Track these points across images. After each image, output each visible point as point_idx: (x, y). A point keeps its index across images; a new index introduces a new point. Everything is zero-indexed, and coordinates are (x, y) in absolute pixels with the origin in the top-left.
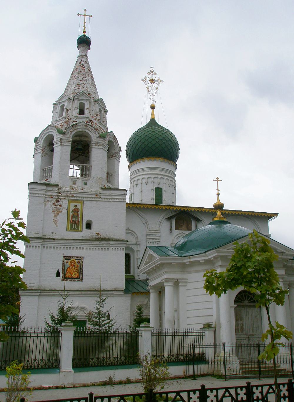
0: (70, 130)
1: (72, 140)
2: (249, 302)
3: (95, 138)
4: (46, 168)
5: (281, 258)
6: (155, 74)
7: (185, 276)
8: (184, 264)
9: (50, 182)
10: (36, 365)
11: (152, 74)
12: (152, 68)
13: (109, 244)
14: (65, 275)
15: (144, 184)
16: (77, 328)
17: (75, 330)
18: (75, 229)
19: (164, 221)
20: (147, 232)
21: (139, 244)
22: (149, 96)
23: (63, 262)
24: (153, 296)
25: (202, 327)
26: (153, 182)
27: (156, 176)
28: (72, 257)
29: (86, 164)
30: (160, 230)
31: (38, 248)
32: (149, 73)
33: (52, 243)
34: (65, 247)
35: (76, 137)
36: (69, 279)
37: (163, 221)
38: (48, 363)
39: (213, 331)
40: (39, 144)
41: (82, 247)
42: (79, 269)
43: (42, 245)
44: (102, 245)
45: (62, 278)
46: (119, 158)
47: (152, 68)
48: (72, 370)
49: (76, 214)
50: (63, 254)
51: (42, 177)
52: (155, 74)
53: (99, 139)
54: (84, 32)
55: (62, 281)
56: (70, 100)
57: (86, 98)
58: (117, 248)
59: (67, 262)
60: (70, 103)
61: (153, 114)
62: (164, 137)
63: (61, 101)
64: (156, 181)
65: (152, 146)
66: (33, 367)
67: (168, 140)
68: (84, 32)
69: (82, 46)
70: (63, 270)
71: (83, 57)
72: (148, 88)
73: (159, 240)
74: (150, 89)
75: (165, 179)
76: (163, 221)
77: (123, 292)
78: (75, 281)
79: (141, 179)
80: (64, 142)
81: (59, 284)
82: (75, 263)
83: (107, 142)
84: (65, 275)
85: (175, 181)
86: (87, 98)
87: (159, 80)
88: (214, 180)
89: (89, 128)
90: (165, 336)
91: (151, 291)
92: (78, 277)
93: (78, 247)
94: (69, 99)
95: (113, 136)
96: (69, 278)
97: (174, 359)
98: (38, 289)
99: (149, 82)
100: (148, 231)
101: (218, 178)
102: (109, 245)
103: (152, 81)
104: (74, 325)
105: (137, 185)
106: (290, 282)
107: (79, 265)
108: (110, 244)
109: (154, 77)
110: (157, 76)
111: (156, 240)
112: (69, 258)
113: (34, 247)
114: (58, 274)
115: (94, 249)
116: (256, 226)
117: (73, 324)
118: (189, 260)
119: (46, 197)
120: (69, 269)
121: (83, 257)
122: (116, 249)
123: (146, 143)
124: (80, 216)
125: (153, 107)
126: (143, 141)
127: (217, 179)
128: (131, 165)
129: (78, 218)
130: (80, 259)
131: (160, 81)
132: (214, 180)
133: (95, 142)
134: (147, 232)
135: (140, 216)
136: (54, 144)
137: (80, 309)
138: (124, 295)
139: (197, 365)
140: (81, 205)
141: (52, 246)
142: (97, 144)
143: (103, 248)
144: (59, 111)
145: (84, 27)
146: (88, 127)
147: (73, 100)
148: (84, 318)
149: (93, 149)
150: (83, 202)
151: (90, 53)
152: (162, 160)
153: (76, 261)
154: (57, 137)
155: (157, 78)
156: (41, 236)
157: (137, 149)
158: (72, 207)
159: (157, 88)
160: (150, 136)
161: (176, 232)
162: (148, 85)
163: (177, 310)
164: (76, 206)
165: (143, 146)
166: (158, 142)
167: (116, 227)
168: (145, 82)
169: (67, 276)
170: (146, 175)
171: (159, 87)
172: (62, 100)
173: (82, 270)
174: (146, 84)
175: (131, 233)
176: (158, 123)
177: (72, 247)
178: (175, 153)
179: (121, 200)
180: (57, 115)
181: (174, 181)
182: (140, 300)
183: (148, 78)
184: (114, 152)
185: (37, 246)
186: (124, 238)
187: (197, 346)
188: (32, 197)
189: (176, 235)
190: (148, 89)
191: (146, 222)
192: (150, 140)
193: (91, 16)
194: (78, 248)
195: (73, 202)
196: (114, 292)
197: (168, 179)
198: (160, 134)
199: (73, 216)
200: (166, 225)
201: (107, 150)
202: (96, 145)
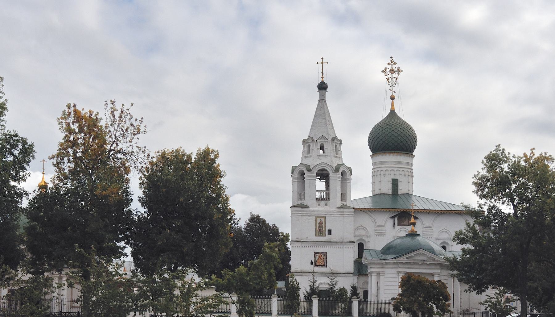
4: (301, 192)
6: (395, 64)
7: (384, 270)
8: (383, 263)
12: (392, 58)
15: (382, 176)
18: (320, 235)
22: (389, 87)
27: (382, 169)
28: (320, 252)
32: (389, 64)
36: (318, 266)
41: (325, 246)
42: (325, 260)
48: (318, 316)
49: (321, 225)
51: (299, 199)
52: (395, 64)
54: (322, 78)
58: (348, 247)
61: (393, 105)
64: (392, 173)
68: (322, 78)
71: (322, 100)
72: (388, 79)
73: (385, 234)
74: (390, 80)
75: (401, 171)
78: (322, 267)
79: (380, 171)
81: (311, 268)
84: (316, 264)
87: (398, 70)
91: (369, 275)
96: (318, 265)
99: (389, 73)
103: (392, 71)
107: (324, 257)
114: (312, 263)
115: (333, 247)
118: (384, 262)
121: (326, 253)
123: (383, 140)
125: (393, 98)
126: (381, 138)
130: (325, 254)
131: (400, 71)
135: (371, 216)
141: (307, 246)
145: (322, 73)
151: (327, 94)
155: (396, 68)
157: (378, 133)
158: (318, 221)
159: (397, 79)
160: (387, 133)
161: (397, 227)
162: (388, 76)
164: (321, 220)
167: (348, 233)
171: (398, 77)
173: (326, 261)
181: (409, 170)
186: (352, 240)
189: (398, 230)
190: (388, 80)
193: (327, 63)
195: (319, 218)
196: (347, 274)
197: (403, 170)
199: (319, 227)
200: (391, 222)
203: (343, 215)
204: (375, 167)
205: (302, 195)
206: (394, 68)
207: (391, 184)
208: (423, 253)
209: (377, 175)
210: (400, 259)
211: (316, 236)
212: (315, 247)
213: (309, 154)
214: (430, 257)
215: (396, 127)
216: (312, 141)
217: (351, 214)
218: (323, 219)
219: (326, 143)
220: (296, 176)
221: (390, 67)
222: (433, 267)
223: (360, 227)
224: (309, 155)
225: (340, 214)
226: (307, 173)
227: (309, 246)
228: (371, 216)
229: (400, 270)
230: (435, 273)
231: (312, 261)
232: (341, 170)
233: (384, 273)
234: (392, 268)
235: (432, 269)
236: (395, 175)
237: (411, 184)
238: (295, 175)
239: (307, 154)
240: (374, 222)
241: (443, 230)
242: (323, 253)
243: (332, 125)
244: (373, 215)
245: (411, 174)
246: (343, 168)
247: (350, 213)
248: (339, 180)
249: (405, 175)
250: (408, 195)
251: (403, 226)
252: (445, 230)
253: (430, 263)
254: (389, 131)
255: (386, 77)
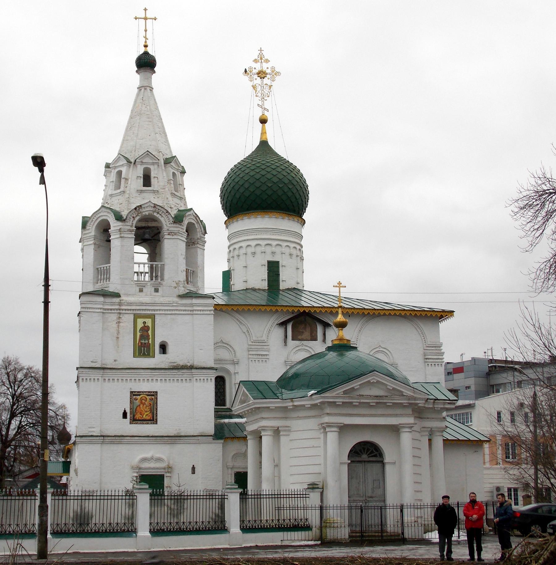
0: (132, 215)
1: (135, 229)
2: (368, 457)
3: (168, 225)
4: (100, 267)
5: (409, 403)
6: (267, 61)
8: (286, 407)
9: (108, 288)
10: (119, 528)
11: (260, 61)
13: (191, 374)
14: (134, 416)
16: (153, 490)
17: (151, 493)
19: (274, 327)
20: (424, 350)
21: (238, 363)
22: (257, 101)
23: (131, 399)
24: (251, 443)
25: (306, 487)
26: (265, 252)
29: (155, 262)
30: (269, 338)
31: (97, 381)
32: (255, 61)
33: (116, 374)
34: (133, 379)
35: (140, 222)
37: (273, 328)
38: (116, 527)
39: (319, 492)
40: (90, 233)
42: (152, 408)
43: (102, 377)
44: (182, 375)
45: (130, 420)
46: (203, 245)
47: (261, 50)
50: (131, 389)
51: (97, 280)
52: (267, 61)
53: (172, 225)
54: (146, 46)
55: (130, 423)
56: (130, 164)
57: (153, 160)
58: (202, 378)
59: (136, 399)
60: (130, 167)
61: (263, 133)
62: (281, 177)
63: (117, 165)
64: (269, 250)
65: (261, 194)
66: (8, 532)
67: (286, 181)
68: (146, 46)
69: (142, 71)
70: (130, 409)
72: (254, 87)
73: (268, 357)
74: (259, 89)
75: (284, 247)
76: (273, 328)
77: (211, 438)
78: (147, 424)
80: (124, 233)
82: (146, 400)
83: (185, 228)
84: (134, 416)
85: (302, 247)
86: (156, 160)
87: (273, 72)
88: (334, 286)
89: (159, 209)
90: (263, 498)
91: (248, 437)
92: (151, 419)
93: (150, 379)
94: (128, 163)
95: (193, 215)
97: (210, 526)
98: (99, 435)
99: (256, 76)
100: (251, 344)
101: (340, 283)
102: (192, 375)
104: (150, 487)
105: (239, 256)
106: (431, 429)
108: (193, 373)
109: (265, 66)
110: (269, 65)
111: (263, 357)
112: (139, 394)
113: (92, 380)
114: (125, 415)
116: (419, 331)
117: (149, 486)
118: (291, 404)
119: (104, 312)
120: (138, 408)
121: (157, 392)
122: (202, 380)
123: (252, 189)
124: (150, 337)
125: (263, 121)
126: (246, 185)
127: (338, 285)
128: (229, 222)
129: (148, 339)
130: (154, 394)
132: (334, 286)
133: (168, 230)
134: (424, 350)
136: (111, 234)
137: (155, 459)
138: (213, 442)
139: (304, 532)
140: (152, 321)
141: (116, 379)
142: (171, 234)
143: (184, 379)
144: (114, 180)
145: (145, 37)
146: (157, 208)
147: (135, 163)
148: (162, 472)
149: (166, 241)
150: (155, 317)
152: (277, 215)
153: (147, 397)
154: (114, 225)
155: (270, 69)
156: (100, 365)
158: (140, 324)
160: (258, 176)
163: (277, 466)
165: (247, 194)
166: (271, 186)
168: (249, 76)
169: (136, 418)
170: (252, 241)
171: (273, 84)
172: (117, 163)
173: (157, 409)
174: (251, 81)
175: (224, 346)
176: (273, 148)
177: (141, 379)
178: (300, 202)
179: (206, 313)
180: (112, 186)
181: (298, 247)
182: (234, 447)
183: (255, 68)
184: (196, 238)
185: (96, 378)
187: (301, 507)
188: (85, 313)
191: (248, 331)
192: (258, 184)
194: (150, 380)
196: (199, 438)
197: (287, 246)
198: (274, 173)
199: (142, 337)
200: (278, 333)
201: (185, 240)
202: (169, 234)
203: (192, 313)
204: (233, 242)
205: (104, 273)
206: (265, 69)
207: (267, 272)
208: (378, 382)
209: (239, 256)
210: (329, 396)
211: (134, 357)
212: (133, 380)
213: (119, 188)
214: (394, 389)
215: (273, 167)
216: (126, 162)
217: (208, 310)
218: (150, 320)
219: (156, 166)
220: (93, 233)
221: (258, 67)
222: (399, 411)
223: (220, 344)
224: (119, 191)
225: (186, 310)
226: (115, 225)
227: (120, 379)
228: (241, 322)
229: (326, 419)
230: (403, 426)
231: (125, 411)
232: (186, 222)
233: (289, 431)
234: (309, 417)
235: (396, 415)
236: (273, 253)
237: (300, 271)
238: (90, 231)
239: (115, 190)
240: (247, 334)
241: (378, 349)
242: (149, 392)
243: (166, 136)
244: (243, 319)
245: (301, 253)
246: (189, 217)
247: (206, 308)
248: (184, 241)
249: (291, 255)
250: (296, 291)
251: (303, 342)
252: (381, 349)
253: (395, 401)
254: (266, 170)
255: (251, 84)
